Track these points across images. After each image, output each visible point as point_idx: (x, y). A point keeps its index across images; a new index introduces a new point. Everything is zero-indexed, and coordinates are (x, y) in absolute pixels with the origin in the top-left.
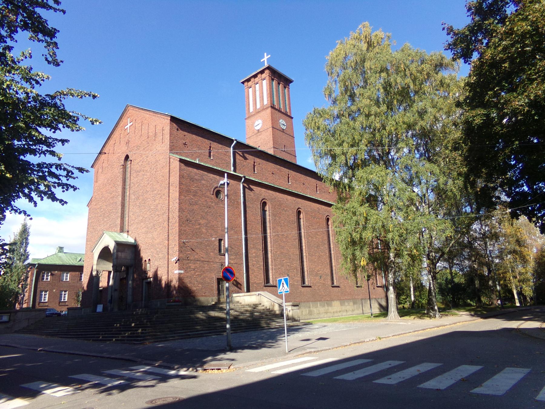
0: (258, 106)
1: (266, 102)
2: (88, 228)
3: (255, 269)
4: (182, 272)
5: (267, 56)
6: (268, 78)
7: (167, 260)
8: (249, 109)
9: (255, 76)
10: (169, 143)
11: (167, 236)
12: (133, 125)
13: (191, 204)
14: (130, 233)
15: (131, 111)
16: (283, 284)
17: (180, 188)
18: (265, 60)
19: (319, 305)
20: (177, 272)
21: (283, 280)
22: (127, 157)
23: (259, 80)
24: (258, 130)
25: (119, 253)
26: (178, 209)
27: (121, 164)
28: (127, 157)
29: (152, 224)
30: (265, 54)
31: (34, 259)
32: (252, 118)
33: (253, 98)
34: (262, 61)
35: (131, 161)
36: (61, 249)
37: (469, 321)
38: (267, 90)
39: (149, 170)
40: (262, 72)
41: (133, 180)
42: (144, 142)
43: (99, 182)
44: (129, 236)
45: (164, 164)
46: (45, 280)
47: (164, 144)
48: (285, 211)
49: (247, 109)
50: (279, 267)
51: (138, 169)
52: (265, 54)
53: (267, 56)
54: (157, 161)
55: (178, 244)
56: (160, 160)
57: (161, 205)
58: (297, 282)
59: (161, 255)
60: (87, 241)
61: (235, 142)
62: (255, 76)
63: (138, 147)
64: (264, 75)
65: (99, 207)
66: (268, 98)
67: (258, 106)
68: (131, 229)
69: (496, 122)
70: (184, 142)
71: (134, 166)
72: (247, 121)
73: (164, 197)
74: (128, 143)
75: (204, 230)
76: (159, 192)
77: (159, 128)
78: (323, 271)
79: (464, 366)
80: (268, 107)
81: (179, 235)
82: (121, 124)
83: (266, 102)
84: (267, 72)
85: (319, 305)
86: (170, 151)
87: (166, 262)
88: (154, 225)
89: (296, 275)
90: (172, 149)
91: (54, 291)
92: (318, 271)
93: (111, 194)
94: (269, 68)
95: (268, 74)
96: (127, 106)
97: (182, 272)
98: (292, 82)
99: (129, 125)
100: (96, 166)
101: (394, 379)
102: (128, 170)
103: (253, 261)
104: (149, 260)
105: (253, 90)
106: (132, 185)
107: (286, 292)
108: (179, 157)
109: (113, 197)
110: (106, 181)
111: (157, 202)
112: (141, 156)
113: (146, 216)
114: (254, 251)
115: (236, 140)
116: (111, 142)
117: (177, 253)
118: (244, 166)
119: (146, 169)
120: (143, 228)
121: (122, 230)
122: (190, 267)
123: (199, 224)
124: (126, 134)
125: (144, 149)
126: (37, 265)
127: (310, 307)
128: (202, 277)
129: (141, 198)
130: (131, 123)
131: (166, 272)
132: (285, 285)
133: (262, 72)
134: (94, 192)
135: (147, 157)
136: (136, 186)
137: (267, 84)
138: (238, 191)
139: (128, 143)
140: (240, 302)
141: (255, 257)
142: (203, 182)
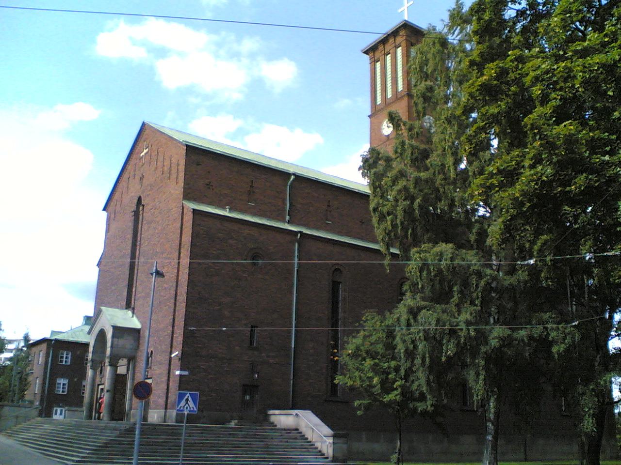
0: (389, 95)
4: (186, 373)
6: (404, 44)
12: (148, 151)
14: (135, 311)
16: (187, 400)
19: (364, 437)
20: (178, 373)
21: (188, 395)
22: (140, 199)
23: (391, 47)
24: (388, 136)
25: (115, 339)
28: (140, 199)
34: (400, 11)
35: (143, 206)
39: (160, 222)
43: (110, 232)
44: (134, 315)
46: (64, 363)
56: (172, 209)
61: (293, 177)
64: (399, 39)
67: (389, 95)
69: (571, 191)
70: (207, 181)
71: (147, 215)
74: (142, 179)
76: (169, 256)
83: (400, 88)
84: (402, 33)
85: (364, 437)
86: (184, 196)
90: (189, 194)
91: (76, 380)
95: (404, 38)
97: (186, 373)
105: (381, 66)
107: (190, 411)
126: (53, 342)
128: (218, 382)
130: (147, 150)
132: (191, 403)
133: (395, 33)
139: (142, 179)
140: (276, 423)
142: (231, 241)
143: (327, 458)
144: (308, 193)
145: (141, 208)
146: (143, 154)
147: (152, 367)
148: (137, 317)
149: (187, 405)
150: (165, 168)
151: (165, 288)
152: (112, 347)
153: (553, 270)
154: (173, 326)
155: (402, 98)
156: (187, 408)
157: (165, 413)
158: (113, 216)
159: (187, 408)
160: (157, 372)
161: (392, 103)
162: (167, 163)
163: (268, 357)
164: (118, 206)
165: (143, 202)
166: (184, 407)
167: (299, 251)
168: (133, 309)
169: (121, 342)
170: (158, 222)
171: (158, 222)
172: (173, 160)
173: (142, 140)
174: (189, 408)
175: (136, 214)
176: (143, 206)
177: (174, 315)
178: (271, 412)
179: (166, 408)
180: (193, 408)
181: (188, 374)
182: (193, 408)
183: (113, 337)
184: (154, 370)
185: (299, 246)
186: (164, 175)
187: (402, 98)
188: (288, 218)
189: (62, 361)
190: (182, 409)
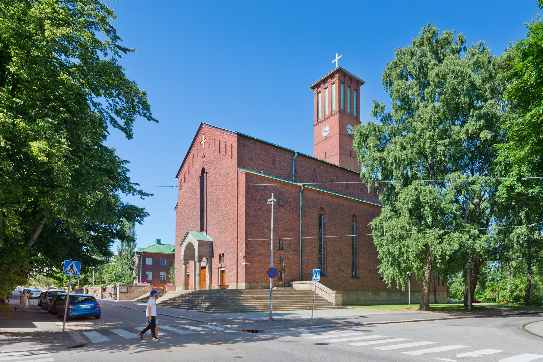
0: (327, 113)
1: (335, 107)
2: (176, 227)
3: (310, 263)
4: (248, 264)
5: (338, 57)
6: (337, 82)
7: (236, 254)
8: (318, 115)
9: (324, 81)
10: (236, 158)
11: (236, 236)
13: (255, 210)
14: (208, 232)
15: (205, 129)
17: (246, 197)
18: (336, 61)
24: (326, 137)
26: (245, 214)
27: (198, 176)
29: (224, 226)
30: (337, 54)
31: (140, 248)
32: (321, 125)
33: (329, 95)
36: (159, 242)
37: (379, 323)
38: (336, 95)
40: (332, 76)
41: (209, 189)
42: (216, 157)
45: (234, 177)
47: (233, 159)
48: (341, 215)
49: (315, 115)
50: (331, 261)
51: (213, 180)
52: (337, 54)
53: (338, 57)
54: (227, 174)
55: (244, 242)
57: (231, 210)
58: (348, 274)
59: (232, 251)
60: (176, 237)
62: (324, 81)
63: (212, 161)
65: (183, 210)
66: (336, 103)
68: (209, 229)
70: (250, 156)
71: (209, 178)
72: (316, 127)
73: (233, 204)
74: (204, 157)
75: (266, 231)
76: (230, 200)
77: (228, 144)
78: (373, 266)
79: (456, 348)
80: (336, 113)
81: (246, 235)
82: (198, 140)
84: (337, 76)
86: (238, 165)
87: (236, 256)
88: (226, 227)
89: (346, 269)
90: (240, 164)
92: (368, 266)
93: (192, 200)
94: (339, 71)
95: (338, 78)
96: (202, 124)
97: (248, 264)
98: (363, 84)
99: (204, 141)
100: (181, 176)
101: (418, 353)
102: (205, 180)
103: (308, 256)
104: (223, 254)
106: (208, 193)
108: (245, 171)
109: (194, 203)
110: (188, 189)
111: (228, 208)
112: (215, 169)
113: (219, 220)
114: (309, 248)
115: (297, 153)
116: (190, 156)
117: (244, 249)
118: (304, 176)
119: (218, 180)
120: (218, 229)
121: (202, 229)
122: (254, 260)
123: (263, 227)
124: (202, 149)
125: (216, 163)
127: (357, 295)
129: (215, 204)
130: (206, 140)
131: (236, 263)
133: (332, 76)
134: (179, 199)
135: (220, 170)
136: (212, 194)
137: (336, 88)
138: (265, 224)
141: (310, 253)
143: (333, 304)
144: (304, 164)
145: (205, 174)
146: (203, 142)
147: (225, 261)
148: (210, 236)
149: (72, 270)
150: (222, 150)
151: (229, 219)
152: (198, 251)
153: (75, 233)
154: (237, 239)
155: (335, 114)
156: (72, 272)
157: (237, 285)
158: (183, 180)
159: (72, 272)
160: (229, 263)
161: (329, 117)
162: (223, 146)
163: (288, 254)
164: (187, 173)
165: (206, 171)
166: (69, 271)
167: (302, 197)
168: (206, 231)
169: (203, 249)
170: (219, 182)
171: (219, 182)
172: (228, 144)
173: (201, 134)
174: (73, 272)
175: (202, 178)
176: (207, 173)
177: (237, 233)
178: (293, 282)
179: (237, 282)
180: (77, 272)
181: (147, 263)
182: (77, 272)
183: (199, 246)
184: (226, 263)
185: (302, 194)
186: (221, 154)
187: (335, 114)
188: (294, 178)
189: (164, 260)
190: (67, 272)
